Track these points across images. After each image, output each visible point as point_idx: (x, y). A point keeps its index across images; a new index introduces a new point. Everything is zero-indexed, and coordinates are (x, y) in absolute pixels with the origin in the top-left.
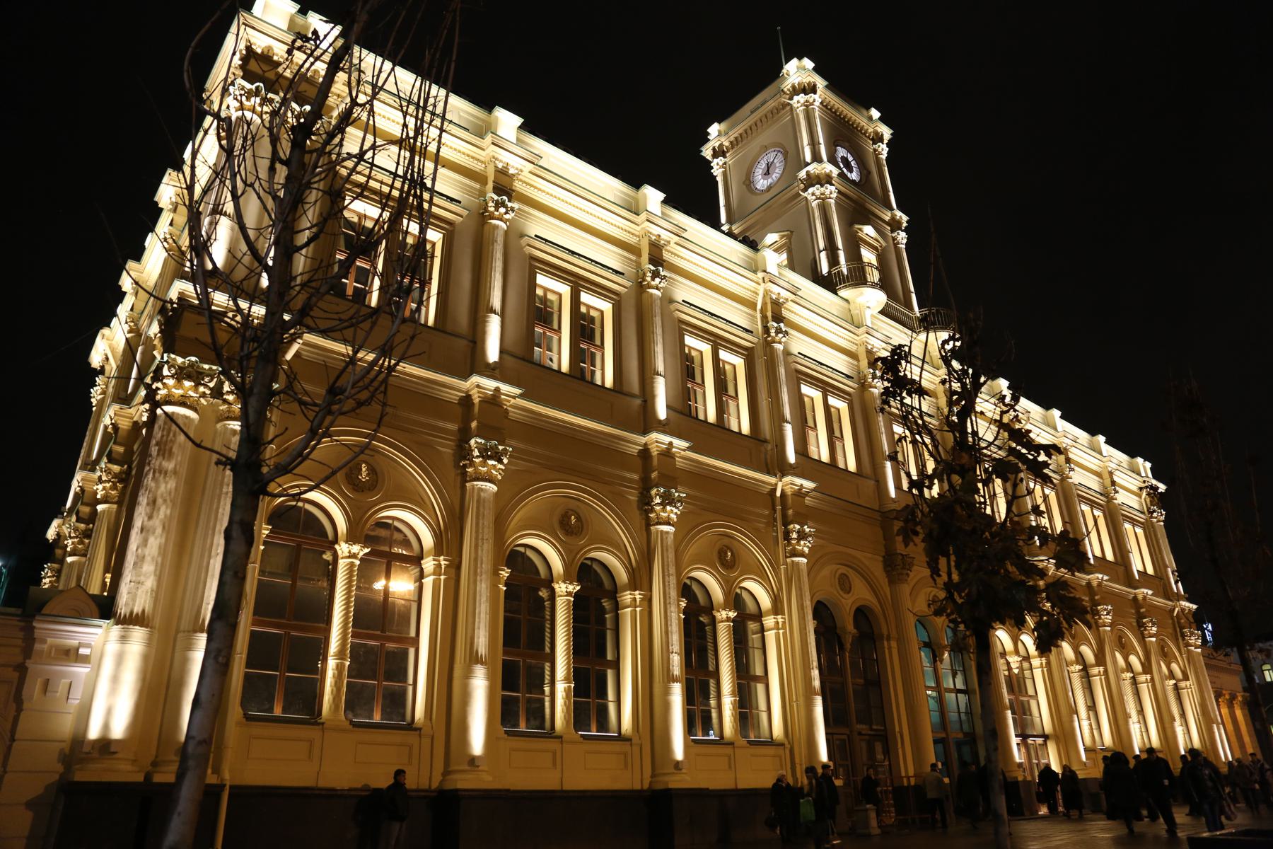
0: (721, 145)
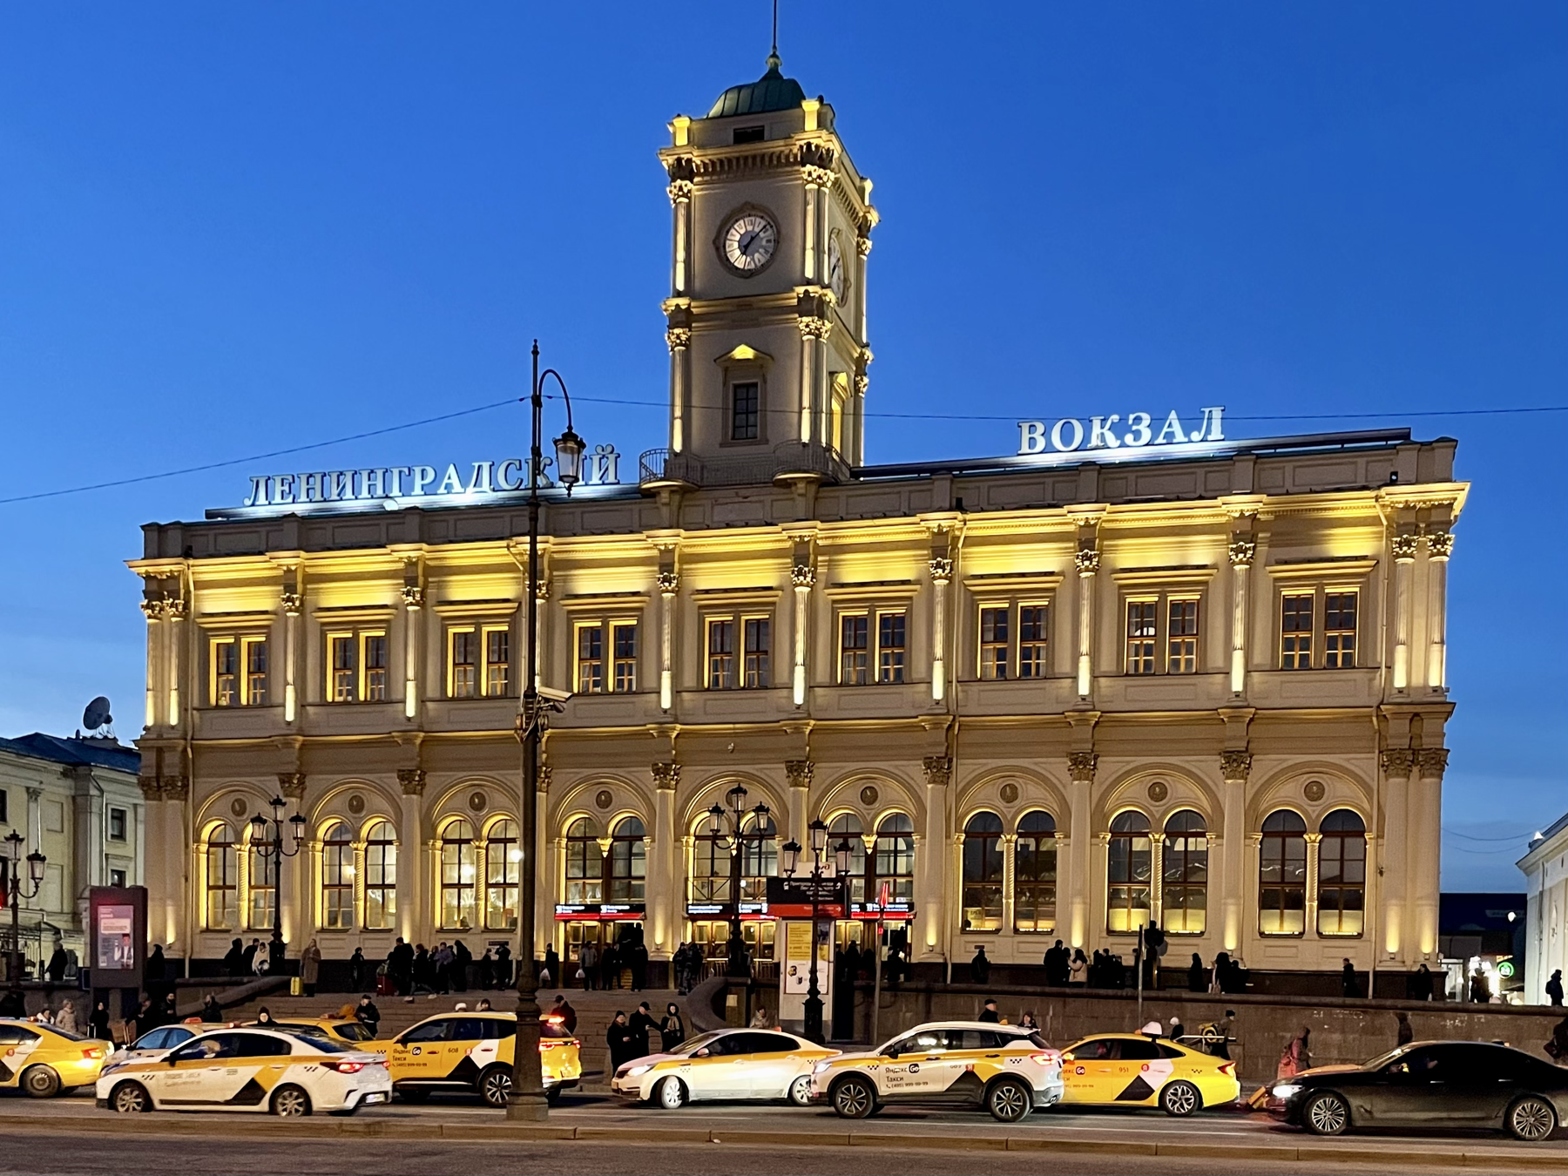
0: (689, 161)
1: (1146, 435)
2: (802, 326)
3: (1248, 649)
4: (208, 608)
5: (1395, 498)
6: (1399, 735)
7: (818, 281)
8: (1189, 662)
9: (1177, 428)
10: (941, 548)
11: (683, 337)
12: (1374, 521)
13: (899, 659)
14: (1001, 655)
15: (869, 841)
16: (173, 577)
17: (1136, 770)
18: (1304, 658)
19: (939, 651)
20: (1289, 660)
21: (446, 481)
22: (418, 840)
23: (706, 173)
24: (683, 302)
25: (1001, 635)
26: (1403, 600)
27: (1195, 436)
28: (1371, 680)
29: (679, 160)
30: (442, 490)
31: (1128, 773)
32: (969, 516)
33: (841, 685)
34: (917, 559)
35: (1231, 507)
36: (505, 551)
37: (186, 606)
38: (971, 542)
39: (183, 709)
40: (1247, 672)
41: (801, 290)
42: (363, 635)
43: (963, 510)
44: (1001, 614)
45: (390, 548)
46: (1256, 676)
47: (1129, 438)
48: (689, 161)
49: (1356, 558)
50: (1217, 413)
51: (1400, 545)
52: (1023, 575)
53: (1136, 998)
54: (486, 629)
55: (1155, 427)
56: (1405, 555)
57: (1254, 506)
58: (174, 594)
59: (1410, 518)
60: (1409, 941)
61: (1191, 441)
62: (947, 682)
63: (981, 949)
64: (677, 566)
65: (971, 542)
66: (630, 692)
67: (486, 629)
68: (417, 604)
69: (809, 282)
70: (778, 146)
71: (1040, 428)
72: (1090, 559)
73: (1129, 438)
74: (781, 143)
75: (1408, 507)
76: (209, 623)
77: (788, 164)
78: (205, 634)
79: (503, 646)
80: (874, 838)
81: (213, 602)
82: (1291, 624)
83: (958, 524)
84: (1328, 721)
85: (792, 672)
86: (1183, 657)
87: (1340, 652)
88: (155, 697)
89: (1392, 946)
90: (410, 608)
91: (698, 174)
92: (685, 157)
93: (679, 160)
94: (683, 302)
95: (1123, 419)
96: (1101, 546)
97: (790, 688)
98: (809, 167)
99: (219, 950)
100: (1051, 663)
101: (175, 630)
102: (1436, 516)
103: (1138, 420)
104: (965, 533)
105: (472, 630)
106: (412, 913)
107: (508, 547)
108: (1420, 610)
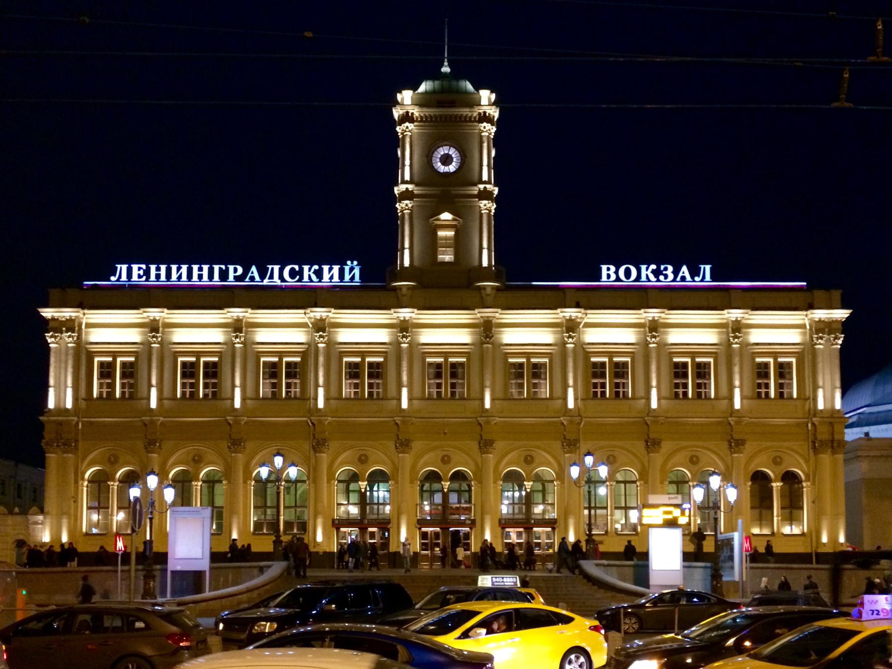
0: (412, 113)
1: (671, 277)
2: (482, 205)
3: (327, 386)
4: (93, 339)
5: (399, 315)
6: (823, 434)
7: (489, 182)
8: (378, 393)
9: (256, 275)
10: (571, 326)
11: (410, 206)
12: (803, 326)
13: (131, 386)
14: (274, 385)
15: (446, 484)
16: (71, 320)
17: (603, 447)
18: (439, 393)
19: (154, 382)
20: (676, 395)
21: (250, 274)
22: (241, 481)
23: (421, 121)
24: (410, 187)
25: (520, 376)
26: (820, 366)
27: (697, 279)
28: (804, 405)
29: (407, 113)
30: (247, 279)
31: (760, 451)
32: (589, 311)
33: (428, 399)
34: (554, 333)
35: (399, 315)
36: (303, 316)
37: (79, 337)
38: (588, 325)
39: (76, 399)
40: (659, 399)
41: (482, 186)
42: (119, 360)
43: (83, 308)
44: (274, 365)
45: (226, 310)
46: (415, 402)
47: (662, 278)
48: (412, 113)
49: (793, 344)
50: (708, 268)
51: (817, 339)
52: (781, 344)
53: (116, 571)
54: (202, 359)
55: (676, 273)
56: (820, 344)
57: (742, 315)
58: (71, 329)
59: (822, 326)
60: (833, 538)
61: (694, 281)
62: (576, 399)
63: (629, 542)
64: (161, 329)
65: (588, 325)
66: (378, 399)
67: (285, 359)
68: (241, 343)
69: (485, 183)
70: (465, 111)
71: (163, 268)
72: (157, 337)
73: (662, 278)
74: (468, 110)
75: (820, 321)
76: (94, 348)
77: (470, 121)
78: (90, 356)
79: (129, 371)
80: (200, 483)
81: (96, 336)
82: (677, 375)
83: (82, 316)
84: (783, 425)
85: (149, 391)
86: (375, 390)
87: (621, 390)
88: (55, 391)
89: (825, 539)
90: (70, 345)
91: (417, 121)
92: (411, 111)
93: (407, 113)
94: (410, 187)
95: (658, 267)
96: (329, 332)
97: (232, 399)
98: (485, 124)
99: (93, 547)
100: (385, 390)
101: (71, 352)
102: (69, 324)
103: (666, 269)
104: (586, 320)
105: (382, 359)
106: (239, 524)
107: (305, 313)
108: (827, 371)
